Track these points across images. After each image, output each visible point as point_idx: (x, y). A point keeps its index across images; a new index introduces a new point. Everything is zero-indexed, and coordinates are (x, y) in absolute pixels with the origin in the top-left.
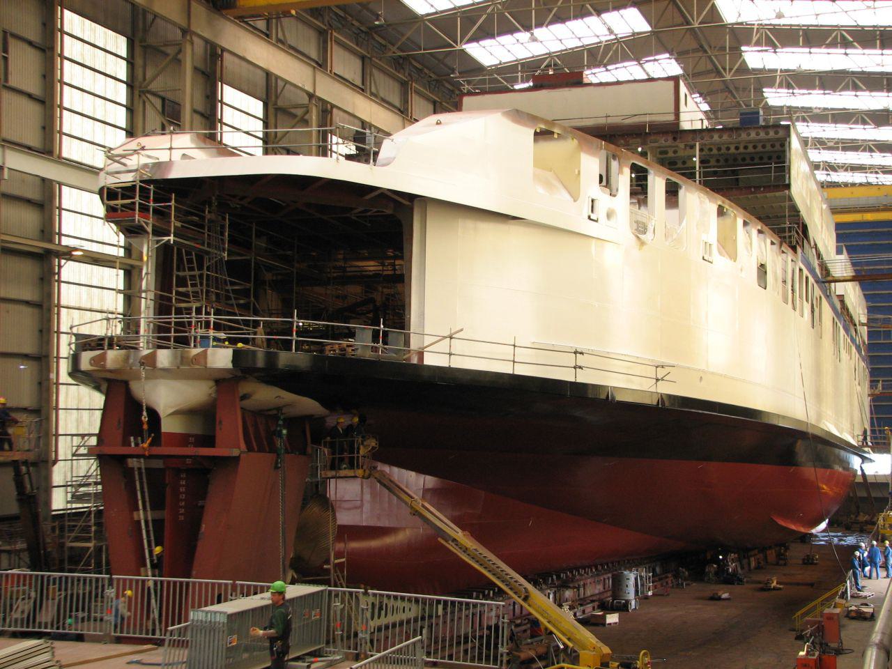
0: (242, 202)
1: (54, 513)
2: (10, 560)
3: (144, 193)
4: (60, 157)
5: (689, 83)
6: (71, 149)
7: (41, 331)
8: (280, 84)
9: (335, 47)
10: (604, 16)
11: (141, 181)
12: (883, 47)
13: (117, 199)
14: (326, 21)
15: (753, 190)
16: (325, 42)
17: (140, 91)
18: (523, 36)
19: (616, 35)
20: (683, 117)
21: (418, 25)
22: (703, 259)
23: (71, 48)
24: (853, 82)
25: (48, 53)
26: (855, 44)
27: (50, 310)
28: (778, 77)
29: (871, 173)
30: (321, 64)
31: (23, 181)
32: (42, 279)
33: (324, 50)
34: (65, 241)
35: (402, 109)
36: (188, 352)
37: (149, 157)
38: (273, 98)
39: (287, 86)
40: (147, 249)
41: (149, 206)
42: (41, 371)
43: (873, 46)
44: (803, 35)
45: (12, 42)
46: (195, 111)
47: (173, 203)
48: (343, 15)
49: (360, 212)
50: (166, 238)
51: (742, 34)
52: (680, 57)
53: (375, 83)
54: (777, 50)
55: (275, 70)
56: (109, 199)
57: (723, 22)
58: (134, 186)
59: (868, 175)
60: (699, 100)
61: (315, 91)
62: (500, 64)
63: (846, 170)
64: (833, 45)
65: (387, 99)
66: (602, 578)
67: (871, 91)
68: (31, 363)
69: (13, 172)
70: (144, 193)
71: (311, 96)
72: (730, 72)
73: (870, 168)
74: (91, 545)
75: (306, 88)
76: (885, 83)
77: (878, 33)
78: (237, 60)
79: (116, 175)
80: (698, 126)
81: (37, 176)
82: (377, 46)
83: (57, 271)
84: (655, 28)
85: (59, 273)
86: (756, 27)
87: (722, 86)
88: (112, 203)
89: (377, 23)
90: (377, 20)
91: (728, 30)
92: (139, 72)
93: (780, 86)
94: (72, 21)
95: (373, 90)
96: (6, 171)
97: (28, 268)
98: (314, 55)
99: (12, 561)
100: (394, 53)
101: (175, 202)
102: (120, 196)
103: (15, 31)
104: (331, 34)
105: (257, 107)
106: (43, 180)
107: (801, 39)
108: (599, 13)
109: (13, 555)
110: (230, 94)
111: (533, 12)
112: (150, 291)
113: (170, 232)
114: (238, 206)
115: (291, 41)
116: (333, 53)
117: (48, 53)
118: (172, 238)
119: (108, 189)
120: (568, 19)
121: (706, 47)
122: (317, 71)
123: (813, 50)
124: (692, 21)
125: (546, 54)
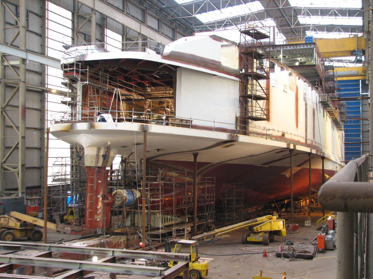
0: (113, 69)
1: (48, 186)
2: (31, 202)
3: (77, 65)
4: (47, 56)
5: (279, 29)
6: (50, 53)
7: (41, 120)
8: (80, 5)
9: (148, 16)
10: (247, 4)
11: (76, 62)
12: (349, 16)
13: (67, 68)
14: (144, 6)
15: (302, 67)
16: (145, 14)
17: (76, 32)
18: (217, 11)
19: (251, 11)
20: (276, 40)
21: (179, 7)
22: (284, 91)
23: (50, 16)
24: (339, 29)
25: (43, 18)
26: (339, 14)
27: (44, 112)
28: (311, 27)
29: (345, 62)
30: (143, 22)
31: (34, 65)
32: (41, 101)
33: (144, 17)
34: (49, 87)
35: (173, 39)
36: (93, 123)
37: (79, 52)
38: (125, 35)
39: (130, 30)
40: (79, 86)
41: (79, 71)
42: (41, 135)
43: (346, 16)
44: (320, 11)
45: (30, 14)
46: (97, 39)
47: (88, 69)
48: (151, 4)
49: (157, 73)
50: (86, 82)
51: (297, 11)
52: (275, 19)
53: (163, 29)
54: (310, 17)
55: (126, 24)
56: (64, 68)
57: (291, 6)
58: (74, 63)
59: (344, 63)
60: (282, 35)
61: (141, 32)
62: (209, 22)
63: (336, 61)
64: (331, 15)
65: (167, 35)
66: (247, 210)
67: (345, 32)
68: (37, 131)
69: (30, 61)
70: (77, 65)
71: (139, 34)
72: (293, 25)
73: (344, 61)
74: (60, 197)
75: (137, 31)
76: (350, 29)
77: (347, 10)
78: (112, 20)
79: (67, 59)
80: (282, 43)
81: (40, 63)
82: (163, 15)
83: (46, 98)
84: (266, 8)
85: (47, 99)
86: (303, 8)
87: (291, 30)
88: (66, 69)
89: (164, 7)
90: (164, 5)
91: (293, 9)
92: (76, 25)
93: (312, 30)
94: (51, 6)
95: (162, 32)
96: (28, 61)
97: (36, 97)
98: (140, 18)
99: (32, 203)
100: (170, 18)
101: (89, 69)
102: (68, 67)
103: (31, 10)
104: (147, 11)
105: (119, 37)
106: (41, 64)
107: (319, 13)
108: (245, 3)
109: (32, 201)
110: (108, 33)
111: (221, 2)
112: (80, 102)
113: (87, 80)
114: (112, 71)
115: (132, 13)
116: (147, 20)
117: (43, 18)
118: (87, 82)
119: (64, 64)
120: (234, 5)
121: (285, 16)
122: (141, 24)
123: (324, 17)
124: (279, 5)
125: (226, 18)
